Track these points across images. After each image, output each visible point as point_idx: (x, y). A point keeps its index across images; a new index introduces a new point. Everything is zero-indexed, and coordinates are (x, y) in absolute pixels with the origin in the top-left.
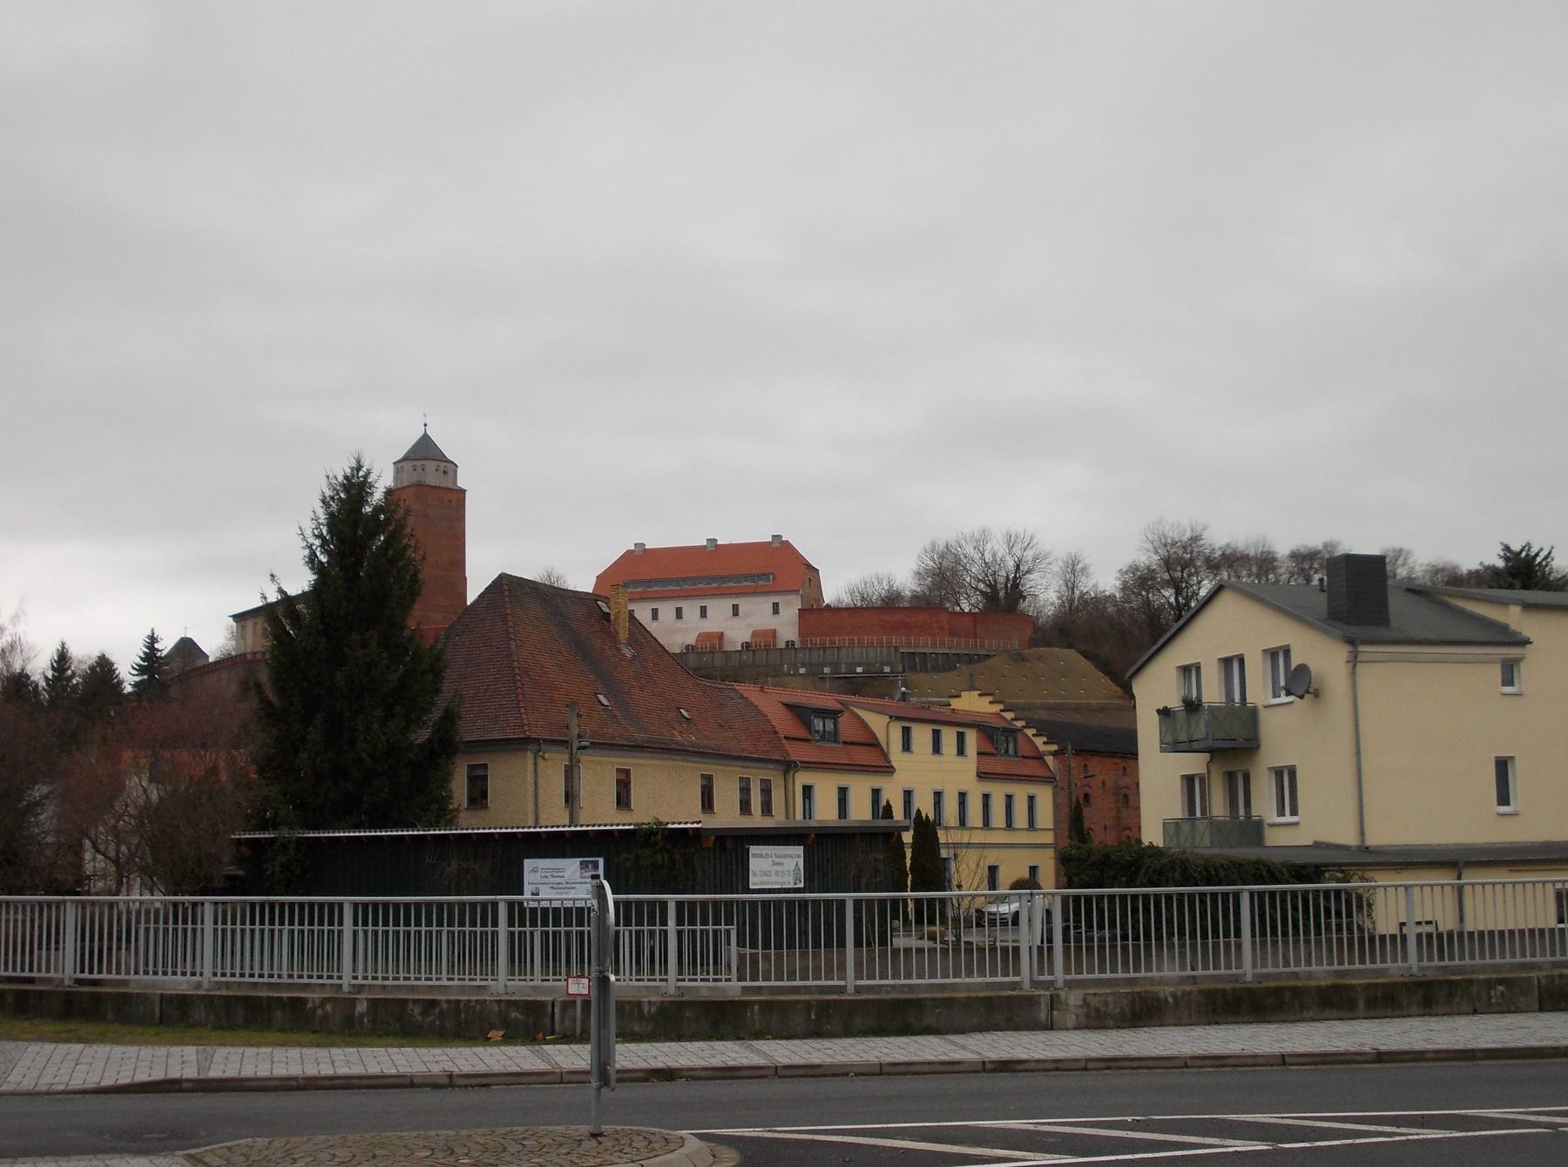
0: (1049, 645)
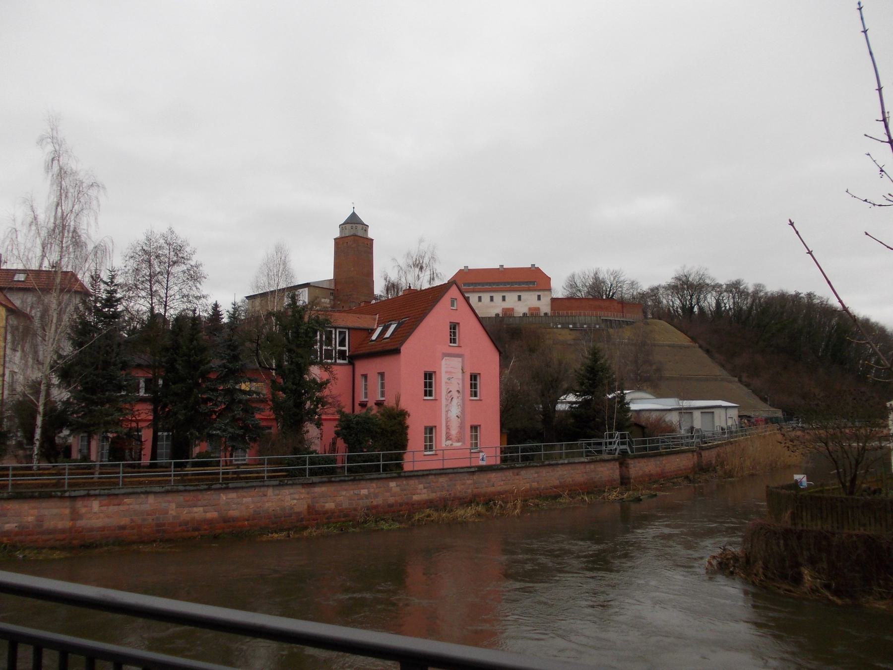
0: (660, 319)
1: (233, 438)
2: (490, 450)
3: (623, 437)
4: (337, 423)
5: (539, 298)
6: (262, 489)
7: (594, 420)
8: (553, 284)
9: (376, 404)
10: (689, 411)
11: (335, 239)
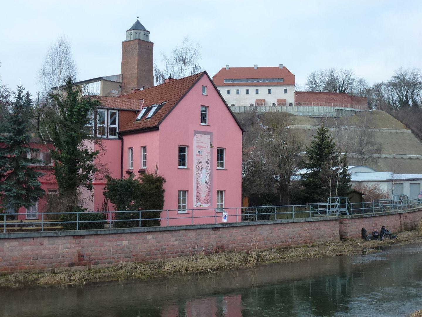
1: (17, 197)
2: (232, 209)
3: (343, 201)
4: (103, 187)
5: (285, 91)
6: (40, 239)
7: (320, 188)
8: (297, 81)
9: (139, 172)
10: (400, 182)
11: (123, 42)
